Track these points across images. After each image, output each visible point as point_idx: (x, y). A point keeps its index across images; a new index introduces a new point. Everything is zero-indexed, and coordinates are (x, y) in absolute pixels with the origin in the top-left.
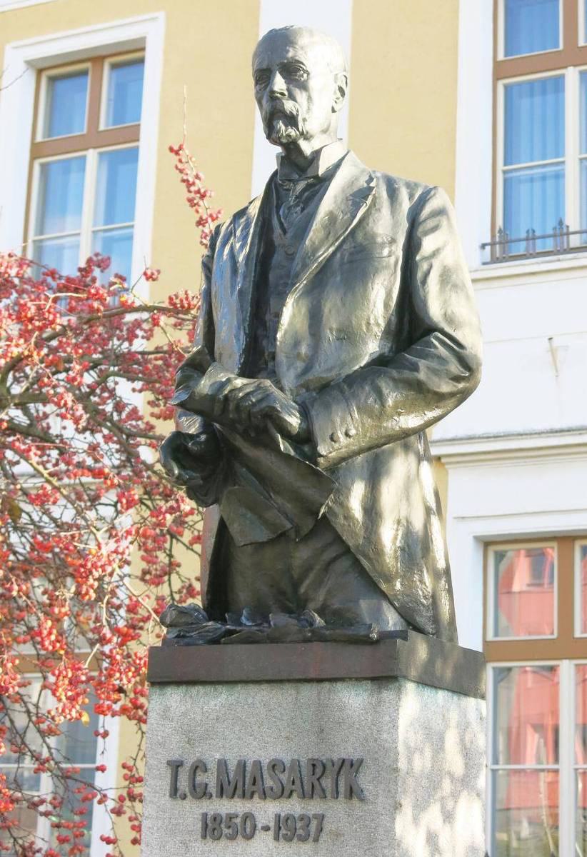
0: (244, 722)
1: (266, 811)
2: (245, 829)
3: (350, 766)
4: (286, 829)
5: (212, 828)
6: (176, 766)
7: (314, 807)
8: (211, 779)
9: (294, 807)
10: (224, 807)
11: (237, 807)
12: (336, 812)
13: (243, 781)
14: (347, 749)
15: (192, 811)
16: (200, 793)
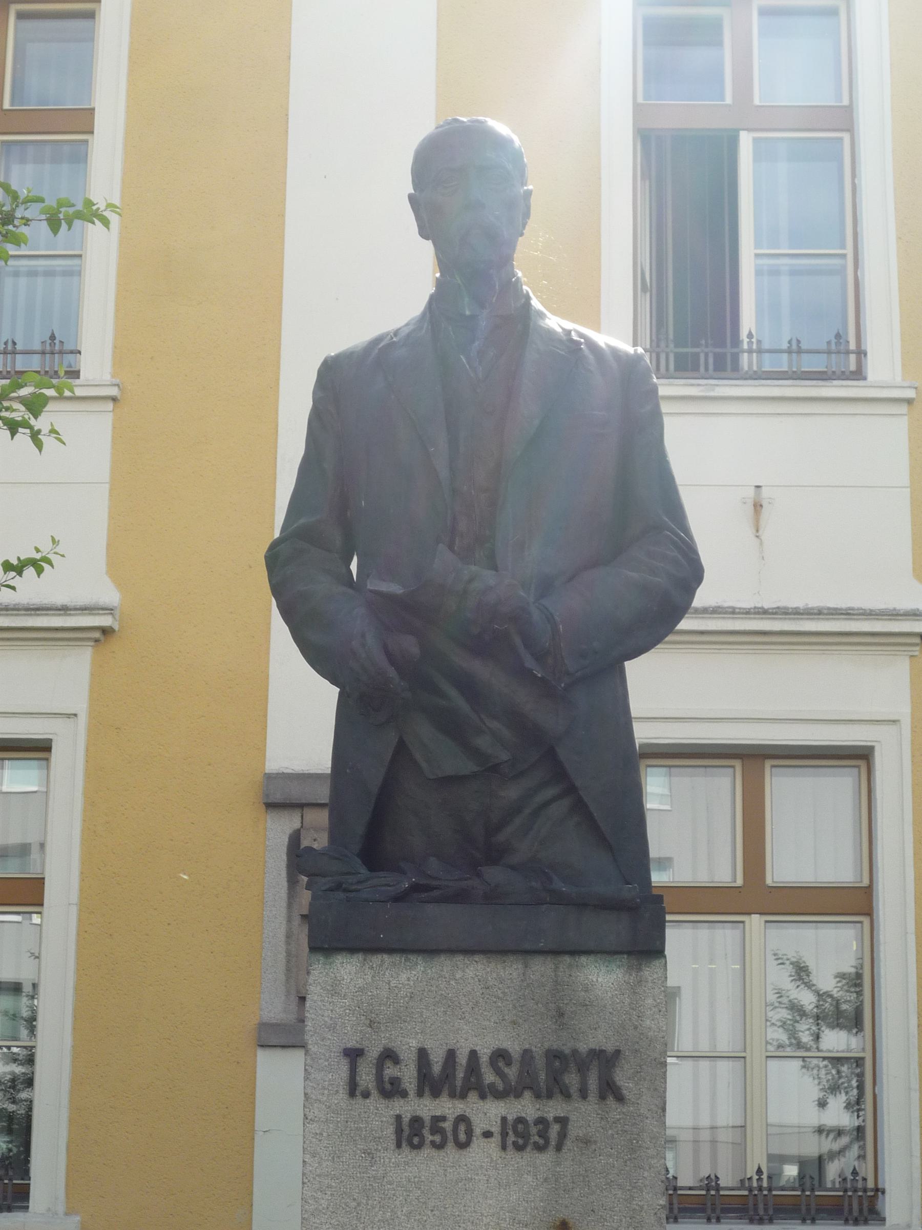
0: (460, 1002)
1: (487, 1113)
2: (460, 1135)
3: (607, 1060)
4: (519, 1137)
5: (411, 1134)
7: (554, 1109)
8: (408, 1074)
9: (527, 1107)
11: (448, 1107)
12: (584, 1115)
15: (380, 1115)
16: (391, 1090)
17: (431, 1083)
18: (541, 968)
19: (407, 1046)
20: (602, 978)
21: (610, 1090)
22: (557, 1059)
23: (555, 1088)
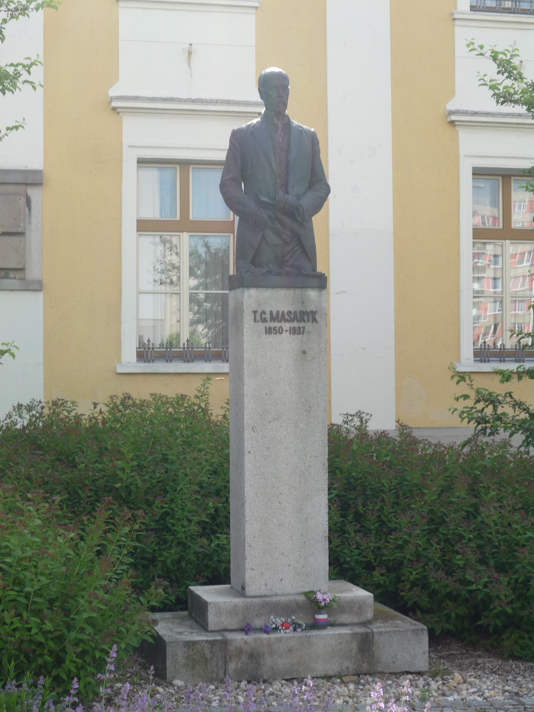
1: (286, 326)
2: (280, 331)
4: (293, 331)
5: (269, 331)
6: (255, 312)
7: (302, 325)
8: (268, 317)
9: (295, 324)
10: (273, 325)
11: (277, 324)
12: (308, 326)
13: (276, 317)
14: (311, 308)
15: (261, 326)
16: (264, 320)
17: (274, 318)
18: (298, 291)
19: (268, 310)
20: (312, 294)
21: (315, 320)
22: (303, 313)
23: (302, 320)
